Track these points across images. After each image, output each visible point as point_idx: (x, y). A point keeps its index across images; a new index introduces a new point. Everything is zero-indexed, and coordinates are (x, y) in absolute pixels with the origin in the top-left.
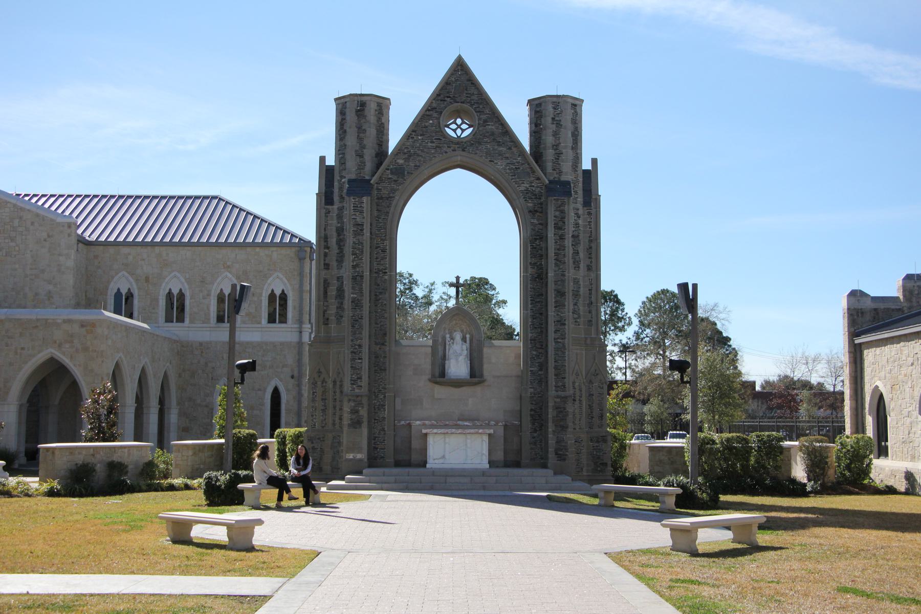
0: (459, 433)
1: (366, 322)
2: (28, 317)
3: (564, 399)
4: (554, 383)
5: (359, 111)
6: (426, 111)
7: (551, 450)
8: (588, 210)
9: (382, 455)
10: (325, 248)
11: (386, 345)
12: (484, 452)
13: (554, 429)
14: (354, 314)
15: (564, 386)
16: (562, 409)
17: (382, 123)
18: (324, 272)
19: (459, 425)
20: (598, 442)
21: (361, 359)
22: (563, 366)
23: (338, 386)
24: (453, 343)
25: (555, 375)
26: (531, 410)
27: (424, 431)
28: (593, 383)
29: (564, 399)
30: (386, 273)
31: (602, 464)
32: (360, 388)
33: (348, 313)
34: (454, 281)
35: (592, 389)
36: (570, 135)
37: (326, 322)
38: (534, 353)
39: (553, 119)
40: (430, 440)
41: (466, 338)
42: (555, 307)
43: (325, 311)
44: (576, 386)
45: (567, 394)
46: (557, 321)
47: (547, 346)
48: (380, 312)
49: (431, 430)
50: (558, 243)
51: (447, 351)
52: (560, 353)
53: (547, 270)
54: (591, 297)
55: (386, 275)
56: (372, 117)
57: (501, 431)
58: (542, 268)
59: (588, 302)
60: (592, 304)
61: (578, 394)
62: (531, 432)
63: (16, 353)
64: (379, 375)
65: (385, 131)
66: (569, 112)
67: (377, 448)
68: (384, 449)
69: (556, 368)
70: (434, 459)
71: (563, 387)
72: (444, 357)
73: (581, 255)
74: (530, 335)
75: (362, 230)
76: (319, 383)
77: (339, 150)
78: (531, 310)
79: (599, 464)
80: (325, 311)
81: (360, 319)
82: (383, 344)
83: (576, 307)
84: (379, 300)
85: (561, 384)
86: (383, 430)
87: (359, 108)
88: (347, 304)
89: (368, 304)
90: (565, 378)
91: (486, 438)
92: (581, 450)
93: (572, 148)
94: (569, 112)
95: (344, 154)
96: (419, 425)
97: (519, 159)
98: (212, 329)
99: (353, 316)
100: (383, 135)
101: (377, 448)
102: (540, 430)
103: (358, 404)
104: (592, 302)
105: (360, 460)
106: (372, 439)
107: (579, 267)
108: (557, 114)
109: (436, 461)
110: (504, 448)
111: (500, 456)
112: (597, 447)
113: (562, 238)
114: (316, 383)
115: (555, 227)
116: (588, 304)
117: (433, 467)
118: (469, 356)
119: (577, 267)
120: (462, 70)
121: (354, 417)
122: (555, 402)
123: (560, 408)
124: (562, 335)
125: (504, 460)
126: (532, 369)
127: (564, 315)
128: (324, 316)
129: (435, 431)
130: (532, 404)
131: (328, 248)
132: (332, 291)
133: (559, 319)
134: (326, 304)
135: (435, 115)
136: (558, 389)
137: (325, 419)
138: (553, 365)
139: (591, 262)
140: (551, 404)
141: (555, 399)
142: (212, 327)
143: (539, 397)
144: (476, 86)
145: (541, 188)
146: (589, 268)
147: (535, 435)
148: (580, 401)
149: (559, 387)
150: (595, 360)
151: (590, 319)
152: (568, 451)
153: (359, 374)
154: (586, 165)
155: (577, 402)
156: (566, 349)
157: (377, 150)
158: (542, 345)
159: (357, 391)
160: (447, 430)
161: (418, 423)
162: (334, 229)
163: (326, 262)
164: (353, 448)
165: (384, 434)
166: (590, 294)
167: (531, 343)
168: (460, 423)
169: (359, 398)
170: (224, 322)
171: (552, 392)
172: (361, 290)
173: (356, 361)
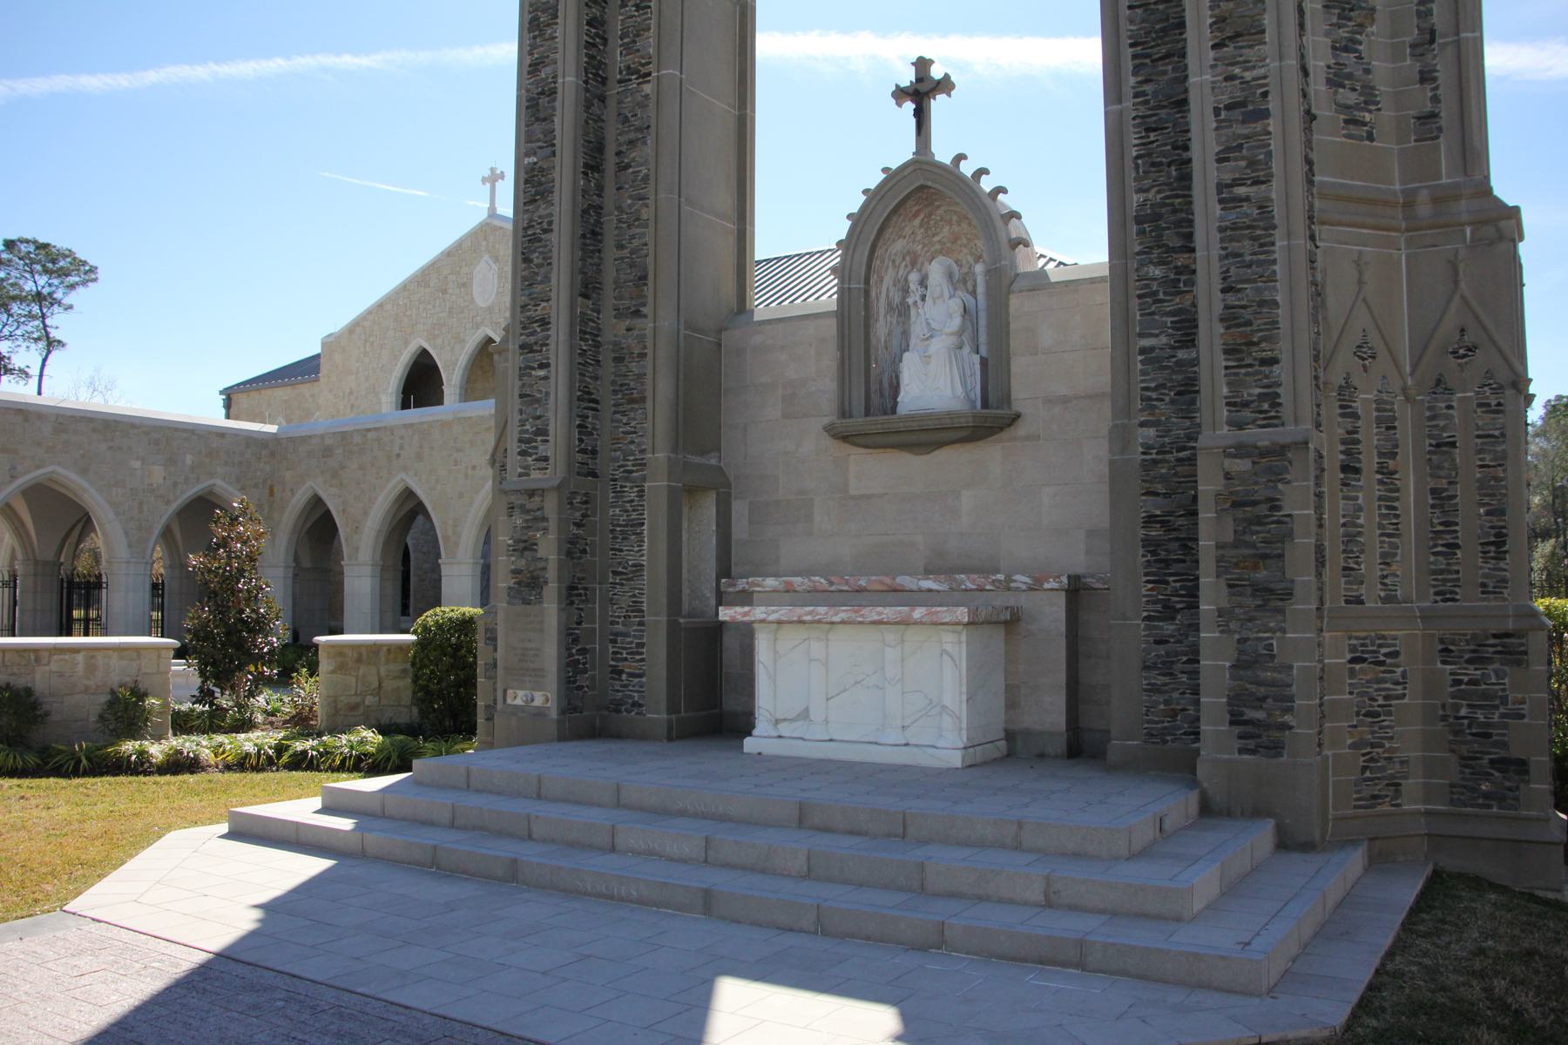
0: (843, 622)
3: (1274, 459)
4: (1225, 390)
7: (1213, 701)
12: (948, 700)
13: (1225, 604)
15: (1273, 399)
16: (1263, 510)
20: (1478, 660)
21: (547, 366)
22: (1262, 303)
25: (1226, 352)
26: (1150, 520)
28: (1450, 391)
29: (1274, 459)
31: (1502, 764)
35: (1450, 417)
38: (1157, 272)
42: (1214, 47)
44: (1358, 406)
45: (1284, 434)
46: (1229, 107)
52: (1246, 247)
54: (1430, 13)
59: (1413, 35)
60: (1432, 41)
61: (1371, 439)
62: (1147, 618)
63: (466, 475)
64: (625, 420)
67: (621, 672)
68: (640, 676)
69: (1230, 318)
70: (777, 722)
71: (1266, 406)
74: (1136, 199)
79: (1485, 761)
82: (637, 313)
83: (1345, 57)
86: (636, 608)
90: (1274, 361)
101: (621, 672)
103: (535, 519)
104: (1432, 33)
105: (540, 713)
106: (572, 638)
112: (1472, 682)
116: (1413, 46)
117: (764, 752)
121: (522, 563)
123: (1254, 503)
124: (1252, 164)
126: (1146, 342)
127: (1256, 73)
130: (1156, 494)
133: (1239, 95)
136: (1247, 414)
138: (1218, 308)
141: (1227, 462)
143: (1179, 460)
147: (1169, 628)
148: (1387, 473)
149: (1246, 404)
150: (1456, 282)
151: (1428, 107)
152: (1290, 710)
153: (539, 417)
155: (1369, 480)
156: (1274, 227)
159: (535, 475)
160: (799, 610)
164: (527, 673)
165: (641, 624)
167: (1141, 233)
169: (537, 499)
171: (1216, 431)
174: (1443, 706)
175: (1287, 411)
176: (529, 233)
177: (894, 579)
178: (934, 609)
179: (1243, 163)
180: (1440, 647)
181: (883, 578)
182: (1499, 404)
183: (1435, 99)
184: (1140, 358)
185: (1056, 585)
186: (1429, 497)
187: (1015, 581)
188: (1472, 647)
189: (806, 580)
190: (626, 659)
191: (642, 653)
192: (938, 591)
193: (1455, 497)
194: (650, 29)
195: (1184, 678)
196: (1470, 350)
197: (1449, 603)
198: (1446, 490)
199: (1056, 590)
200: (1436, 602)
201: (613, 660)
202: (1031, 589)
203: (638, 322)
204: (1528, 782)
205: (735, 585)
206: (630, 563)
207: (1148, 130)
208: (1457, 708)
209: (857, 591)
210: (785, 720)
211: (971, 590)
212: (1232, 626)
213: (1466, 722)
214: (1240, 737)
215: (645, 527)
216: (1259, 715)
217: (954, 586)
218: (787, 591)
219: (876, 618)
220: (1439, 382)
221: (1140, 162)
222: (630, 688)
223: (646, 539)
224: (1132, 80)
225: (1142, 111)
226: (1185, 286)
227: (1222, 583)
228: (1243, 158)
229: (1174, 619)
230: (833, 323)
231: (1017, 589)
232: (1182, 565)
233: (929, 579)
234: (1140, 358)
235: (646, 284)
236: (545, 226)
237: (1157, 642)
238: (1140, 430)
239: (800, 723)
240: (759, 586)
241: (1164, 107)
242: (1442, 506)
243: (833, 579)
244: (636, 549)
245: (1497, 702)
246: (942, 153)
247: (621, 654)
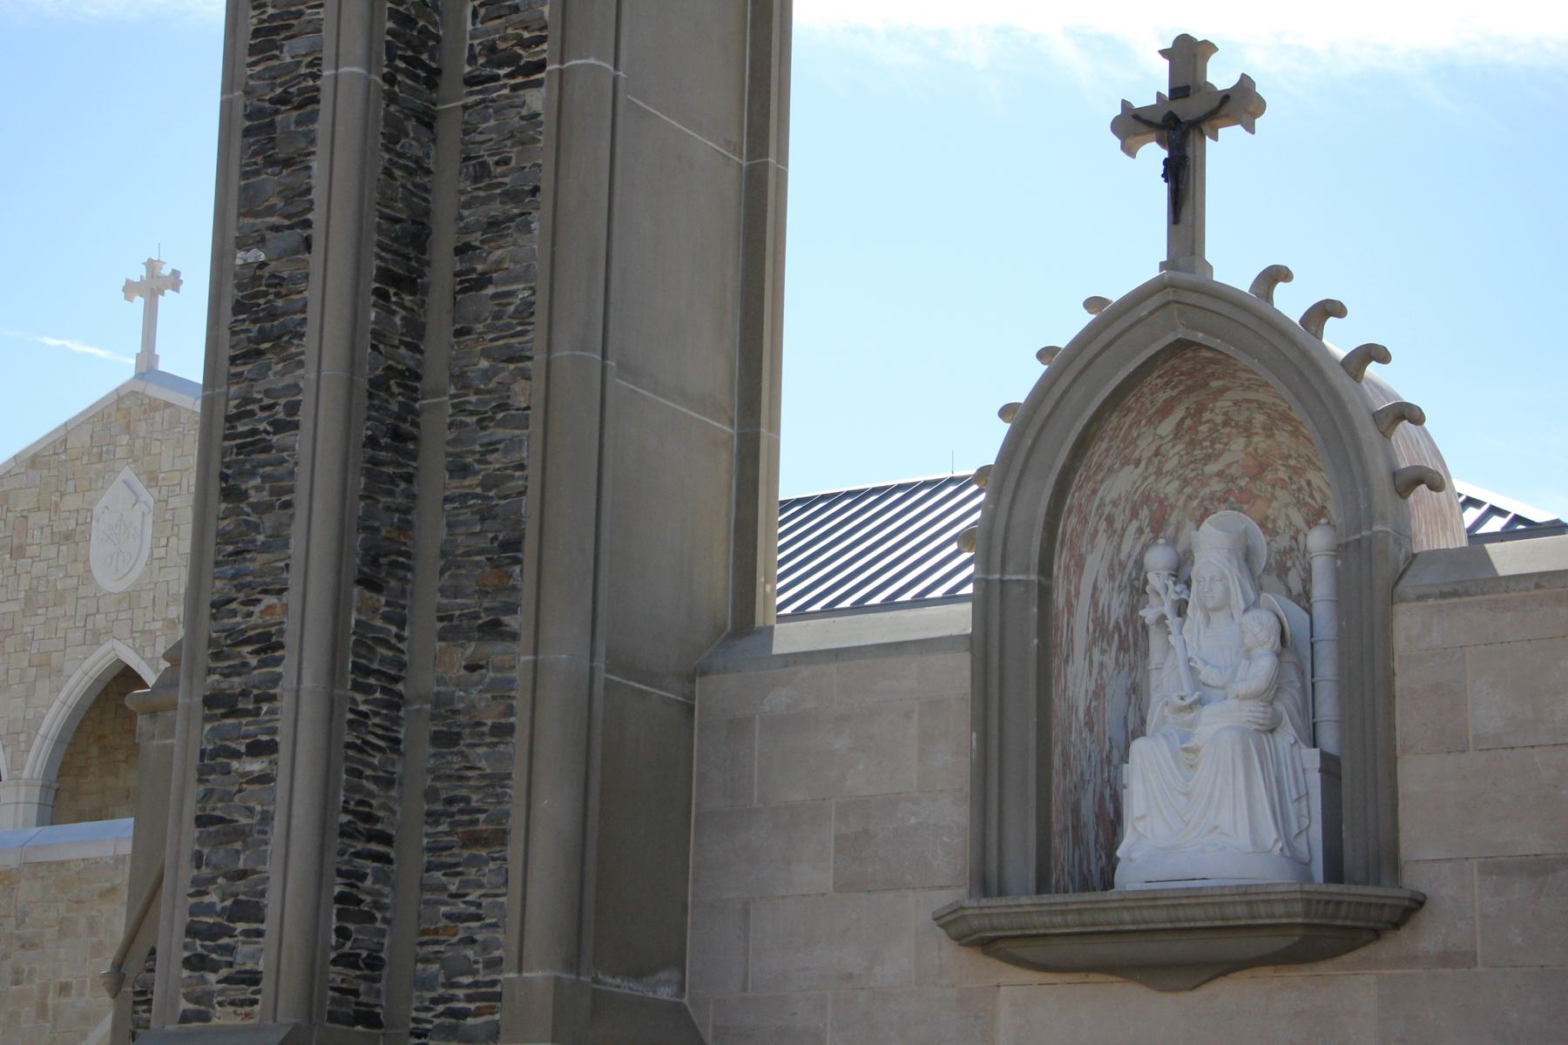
2: (92, 852)
14: (247, 400)
21: (269, 748)
32: (247, 992)
34: (1220, 76)
48: (487, 375)
63: (42, 1010)
82: (494, 629)
99: (240, 416)
153: (243, 874)
203: (495, 650)
230: (962, 664)
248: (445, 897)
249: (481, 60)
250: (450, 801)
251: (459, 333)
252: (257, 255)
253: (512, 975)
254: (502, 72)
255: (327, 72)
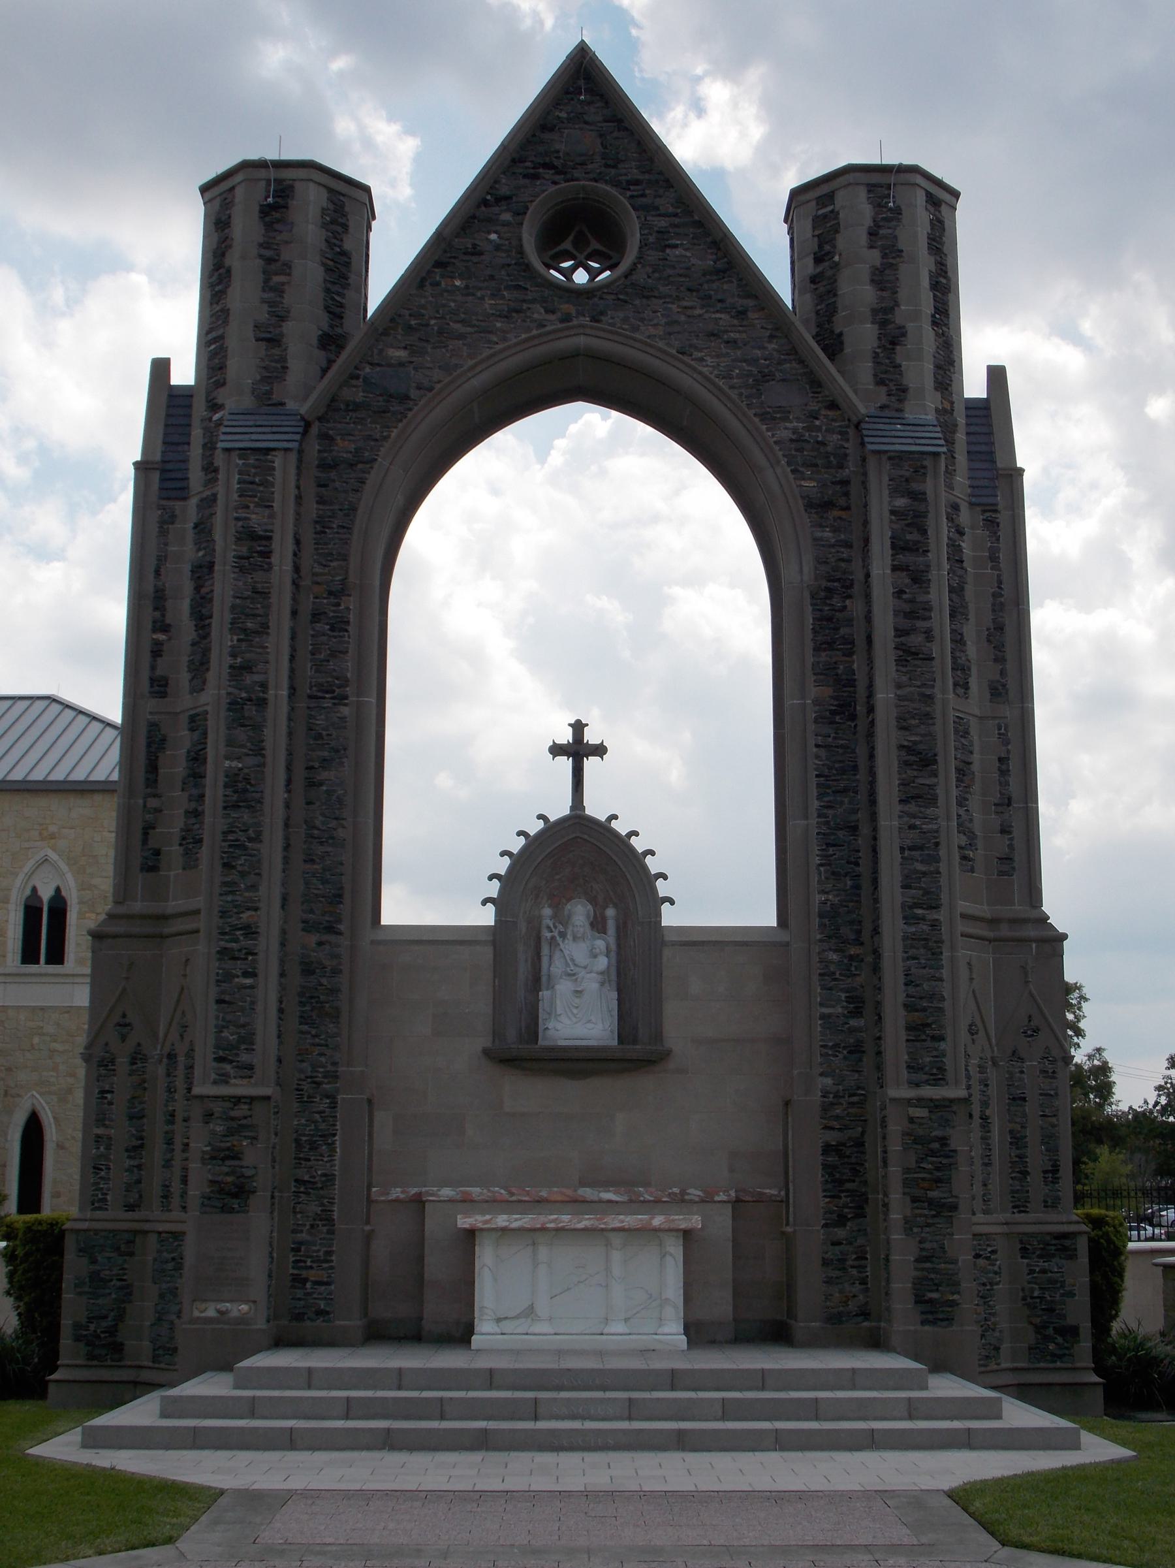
1: (271, 850)
5: (274, 207)
6: (478, 206)
8: (988, 514)
9: (322, 1305)
10: (154, 631)
11: (340, 934)
17: (344, 253)
18: (151, 704)
19: (585, 1201)
20: (1046, 1256)
21: (254, 975)
23: (180, 1071)
24: (563, 935)
27: (464, 1222)
30: (346, 698)
33: (213, 821)
36: (925, 282)
37: (152, 863)
38: (834, 957)
39: (872, 234)
40: (486, 1256)
41: (604, 919)
43: (148, 829)
46: (911, 849)
47: (876, 931)
49: (488, 1217)
50: (905, 596)
51: (545, 961)
53: (870, 686)
55: (346, 705)
56: (310, 227)
57: (722, 1223)
58: (852, 683)
60: (1009, 804)
65: (353, 278)
66: (922, 217)
67: (306, 1280)
68: (328, 1284)
72: (536, 982)
73: (972, 650)
74: (818, 898)
75: (267, 554)
76: (122, 1061)
77: (207, 333)
78: (819, 816)
80: (148, 829)
81: (250, 840)
82: (331, 929)
84: (321, 784)
85: (928, 1059)
87: (270, 200)
88: (214, 790)
89: (281, 795)
90: (941, 1038)
91: (675, 1250)
92: (991, 1284)
93: (935, 323)
94: (922, 217)
95: (221, 337)
96: (451, 1201)
97: (771, 346)
98: (9, 979)
100: (346, 286)
101: (306, 1280)
102: (857, 1216)
104: (1009, 799)
107: (966, 687)
108: (883, 219)
109: (508, 1326)
110: (734, 1280)
111: (720, 1305)
113: (919, 578)
114: (113, 1062)
115: (894, 546)
118: (614, 977)
119: (962, 685)
120: (589, 91)
122: (911, 1120)
125: (735, 1320)
128: (145, 841)
129: (502, 1220)
130: (832, 1128)
131: (165, 628)
132: (175, 765)
134: (153, 803)
135: (507, 217)
137: (139, 1182)
138: (901, 998)
139: (1003, 673)
140: (895, 1128)
142: (9, 975)
143: (852, 1104)
144: (632, 134)
145: (840, 433)
146: (997, 692)
147: (841, 1233)
148: (984, 1118)
153: (243, 1026)
154: (974, 386)
155: (977, 1121)
157: (326, 328)
158: (859, 932)
160: (542, 1219)
161: (447, 1192)
162: (187, 568)
163: (159, 672)
166: (1004, 772)
168: (587, 1193)
170: (37, 962)
172: (258, 750)
173: (237, 980)
174: (1023, 1290)
175: (950, 1075)
176: (230, 838)
177: (576, 1191)
178: (672, 1217)
179: (921, 892)
180: (1020, 1246)
181: (564, 1190)
182: (1054, 1072)
183: (1011, 847)
184: (819, 1022)
185: (725, 1198)
186: (1009, 1137)
187: (689, 1194)
188: (1041, 1246)
189: (485, 1191)
190: (311, 1267)
191: (332, 1261)
192: (617, 1202)
193: (1026, 1137)
194: (347, 652)
195: (854, 1272)
196: (1035, 1032)
197: (1023, 1214)
198: (1019, 1132)
199: (724, 1202)
200: (1014, 1213)
201: (293, 1268)
202: (703, 1201)
203: (332, 938)
204: (1079, 1342)
205: (388, 1194)
206: (319, 1173)
207: (828, 845)
208: (1032, 1290)
209: (538, 1201)
210: (506, 1318)
211: (649, 1201)
212: (915, 1230)
213: (1038, 1300)
214: (922, 1313)
215: (337, 1138)
216: (935, 1295)
217: (633, 1198)
218: (464, 1201)
219: (618, 1225)
220: (1014, 1053)
221: (822, 869)
222: (315, 1296)
223: (338, 1150)
224: (816, 804)
225: (824, 829)
226: (856, 969)
227: (908, 1199)
228: (920, 888)
229: (845, 1226)
230: (488, 952)
231: (691, 1201)
232: (852, 1184)
233: (609, 1191)
234: (819, 1022)
235: (341, 903)
236: (251, 833)
237: (834, 1244)
238: (821, 1079)
239: (523, 1320)
240: (432, 1195)
241: (841, 829)
242: (1017, 1144)
243: (514, 1190)
244: (325, 1159)
245: (1059, 1285)
246: (595, 808)
247: (305, 1262)
248: (309, 1036)
249: (314, 689)
250: (312, 997)
251: (308, 803)
252: (235, 764)
253: (344, 1069)
254: (327, 696)
255: (271, 692)
